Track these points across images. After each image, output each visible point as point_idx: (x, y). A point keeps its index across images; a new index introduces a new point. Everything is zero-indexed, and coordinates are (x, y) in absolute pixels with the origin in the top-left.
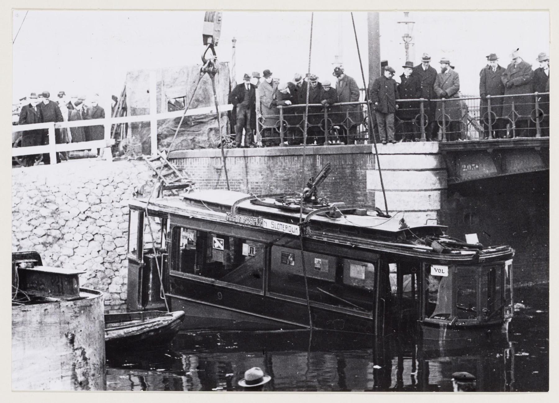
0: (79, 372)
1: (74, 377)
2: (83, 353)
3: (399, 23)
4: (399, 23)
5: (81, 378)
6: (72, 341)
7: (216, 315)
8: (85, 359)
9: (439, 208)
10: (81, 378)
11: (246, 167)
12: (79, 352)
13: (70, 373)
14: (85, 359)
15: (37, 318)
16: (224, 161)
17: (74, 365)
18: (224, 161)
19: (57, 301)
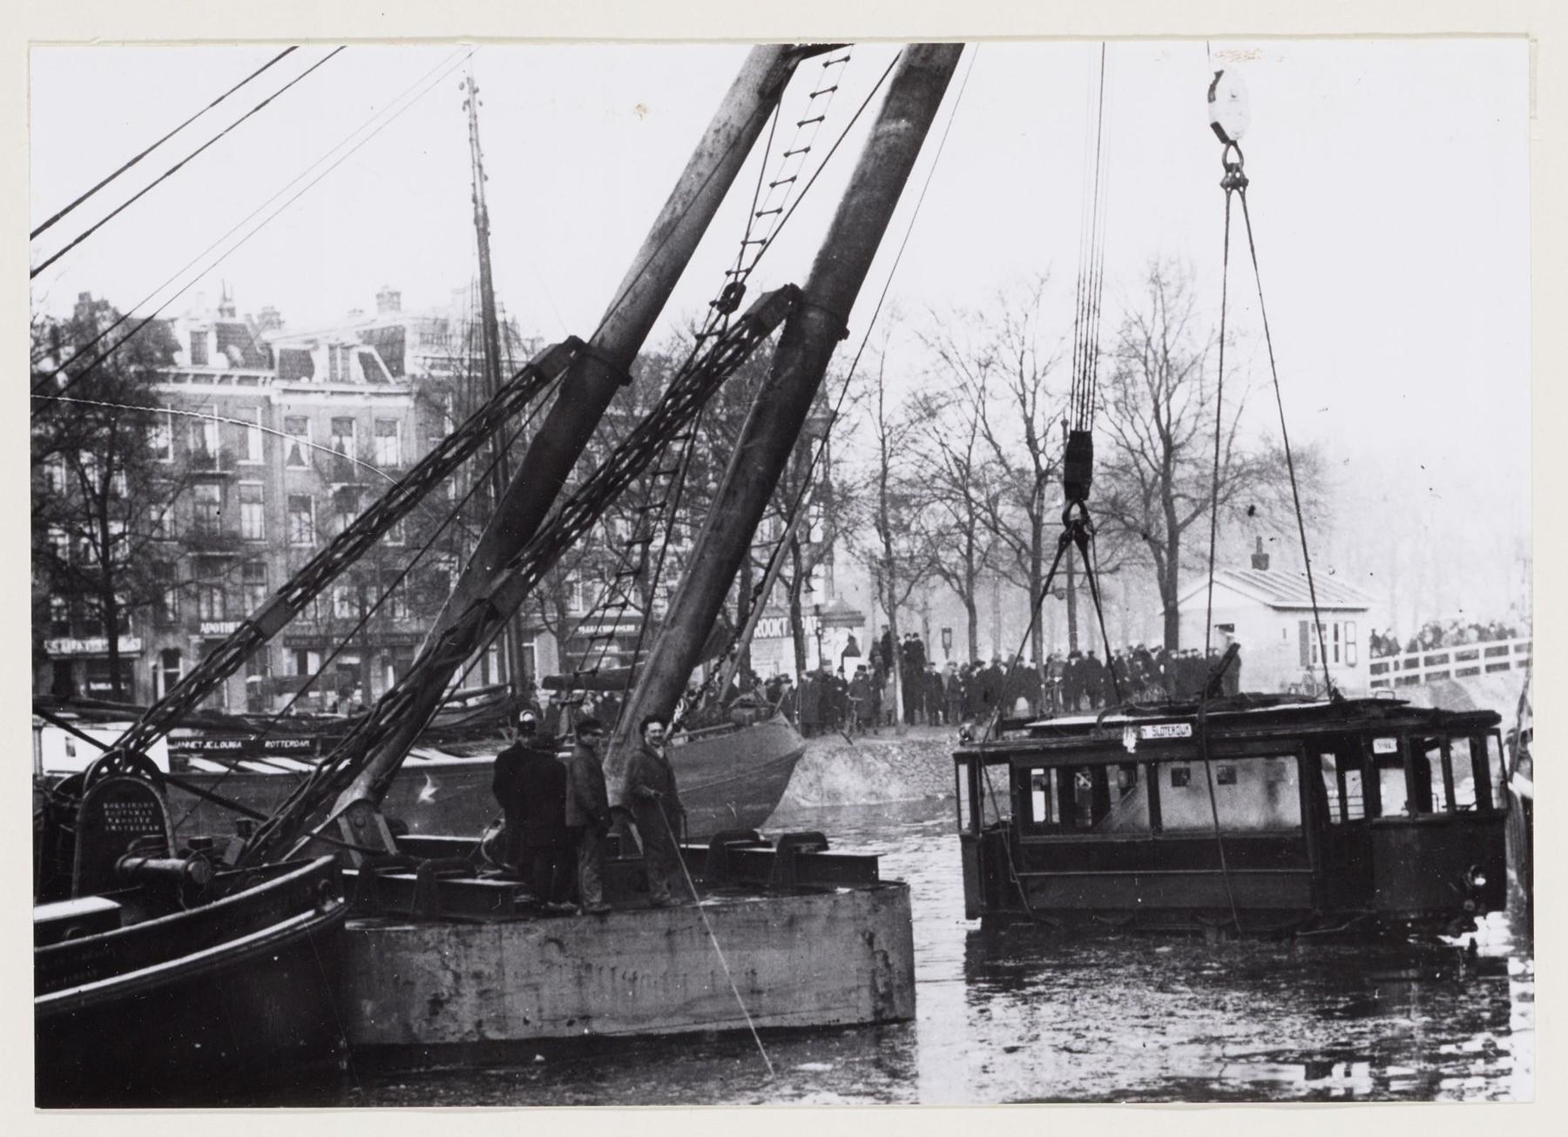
0: (880, 981)
1: (874, 988)
2: (886, 957)
3: (1235, 182)
4: (1235, 182)
5: (882, 990)
6: (870, 941)
7: (736, 595)
8: (888, 966)
9: (1246, 685)
10: (882, 990)
11: (123, 42)
12: (879, 957)
13: (868, 982)
14: (888, 966)
15: (826, 911)
16: (885, 468)
17: (873, 972)
18: (885, 468)
19: (664, 642)
